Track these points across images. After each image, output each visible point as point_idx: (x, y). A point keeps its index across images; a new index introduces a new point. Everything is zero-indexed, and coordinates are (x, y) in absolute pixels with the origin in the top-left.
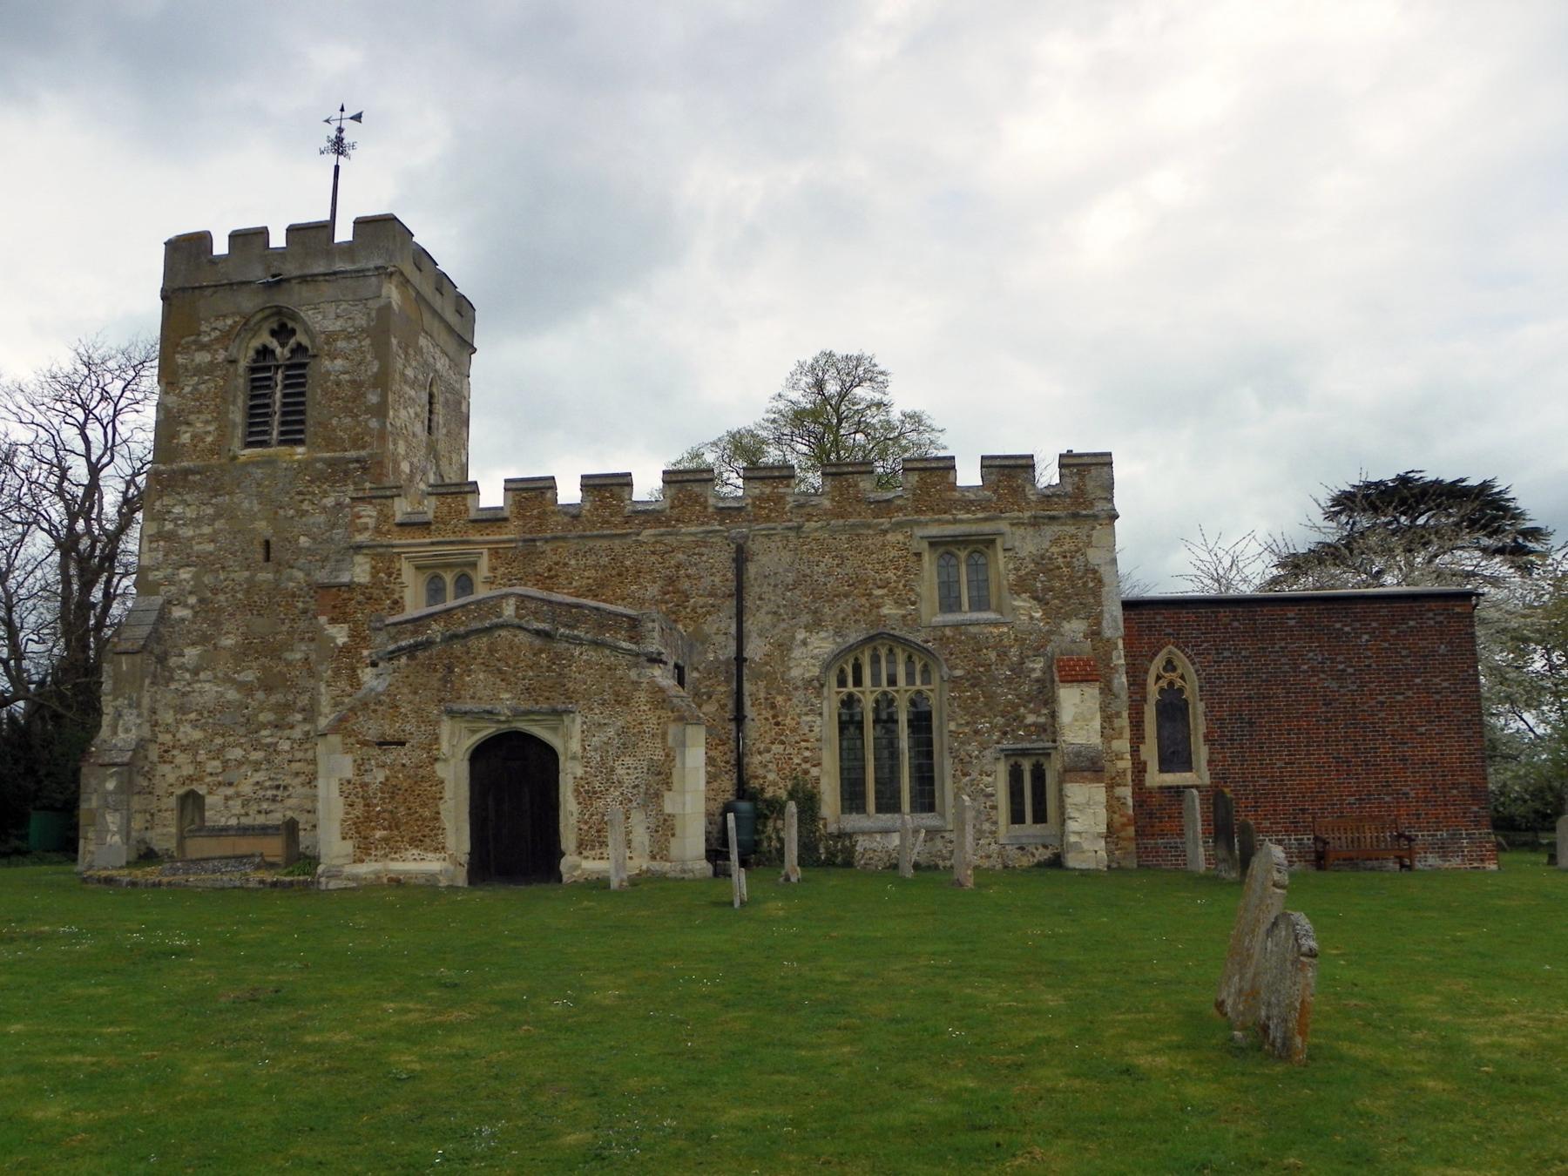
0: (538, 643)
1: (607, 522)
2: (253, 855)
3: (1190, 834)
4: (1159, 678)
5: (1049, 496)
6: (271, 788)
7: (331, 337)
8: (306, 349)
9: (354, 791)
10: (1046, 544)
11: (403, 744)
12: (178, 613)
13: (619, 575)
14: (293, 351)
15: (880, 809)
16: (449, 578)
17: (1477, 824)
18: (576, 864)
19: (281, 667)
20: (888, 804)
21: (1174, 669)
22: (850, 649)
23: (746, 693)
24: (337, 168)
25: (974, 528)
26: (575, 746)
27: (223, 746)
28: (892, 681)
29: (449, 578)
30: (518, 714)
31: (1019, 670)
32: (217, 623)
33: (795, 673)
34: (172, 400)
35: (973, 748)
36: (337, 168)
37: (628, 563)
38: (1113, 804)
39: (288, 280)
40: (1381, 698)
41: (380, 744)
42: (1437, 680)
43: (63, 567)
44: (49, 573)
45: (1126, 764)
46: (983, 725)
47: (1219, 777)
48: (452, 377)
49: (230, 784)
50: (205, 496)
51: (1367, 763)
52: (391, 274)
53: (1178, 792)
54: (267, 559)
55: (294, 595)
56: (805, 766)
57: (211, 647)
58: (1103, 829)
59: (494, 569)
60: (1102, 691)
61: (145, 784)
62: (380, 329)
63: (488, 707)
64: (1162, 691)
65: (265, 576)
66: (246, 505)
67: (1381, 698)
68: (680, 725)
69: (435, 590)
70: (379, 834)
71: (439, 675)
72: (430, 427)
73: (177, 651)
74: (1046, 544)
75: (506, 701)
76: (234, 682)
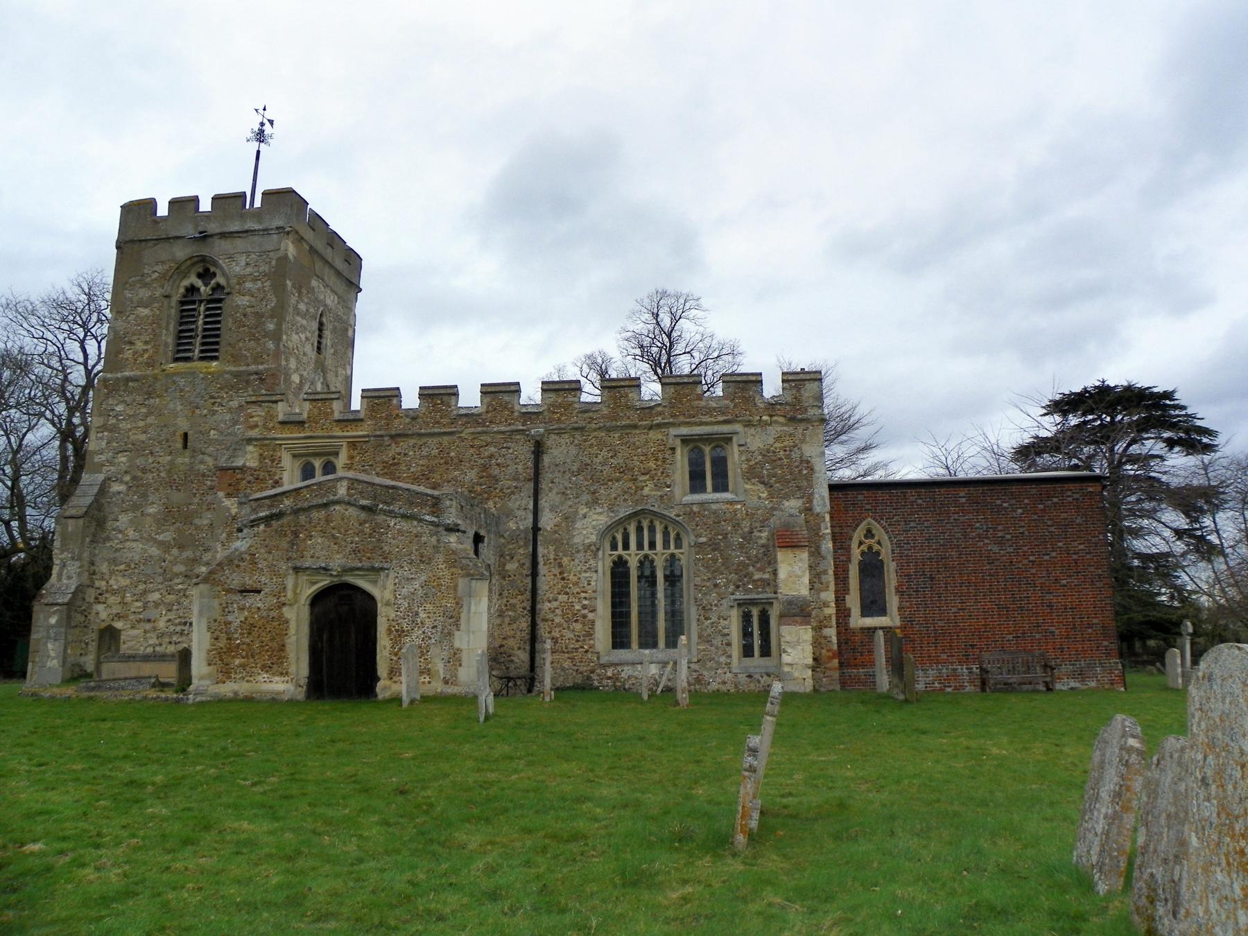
0: (363, 515)
1: (438, 423)
2: (150, 677)
3: (877, 663)
4: (861, 543)
5: (772, 406)
6: (180, 624)
7: (241, 279)
8: (223, 288)
9: (219, 629)
10: (771, 441)
11: (259, 592)
13: (446, 463)
14: (213, 289)
15: (643, 645)
16: (318, 464)
17: (1108, 655)
18: (384, 687)
19: (192, 530)
20: (648, 640)
21: (873, 536)
22: (620, 522)
23: (540, 555)
24: (258, 152)
25: (717, 428)
26: (388, 595)
27: (145, 592)
28: (652, 545)
29: (318, 464)
31: (748, 537)
32: (144, 496)
33: (577, 540)
34: (120, 324)
36: (258, 152)
38: (817, 643)
39: (211, 236)
40: (1032, 558)
41: (241, 592)
42: (1075, 544)
43: (62, 447)
44: (52, 452)
45: (831, 610)
47: (907, 622)
49: (149, 621)
50: (139, 399)
51: (1021, 608)
52: (288, 233)
53: (872, 630)
54: (185, 446)
55: (204, 475)
56: (584, 612)
58: (810, 661)
59: (351, 458)
60: (811, 554)
61: (83, 619)
62: (279, 271)
64: (863, 553)
65: (183, 460)
67: (1032, 558)
68: (467, 579)
69: (308, 472)
70: (237, 662)
72: (319, 348)
73: (112, 516)
74: (771, 441)
75: (337, 561)
76: (155, 540)
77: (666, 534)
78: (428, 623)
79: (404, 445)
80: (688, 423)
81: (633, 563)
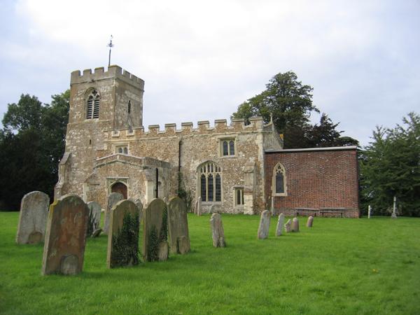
7: (104, 94)
12: (74, 156)
20: (211, 198)
25: (229, 136)
28: (212, 171)
46: (231, 182)
48: (137, 99)
54: (90, 143)
75: (117, 177)
81: (207, 177)
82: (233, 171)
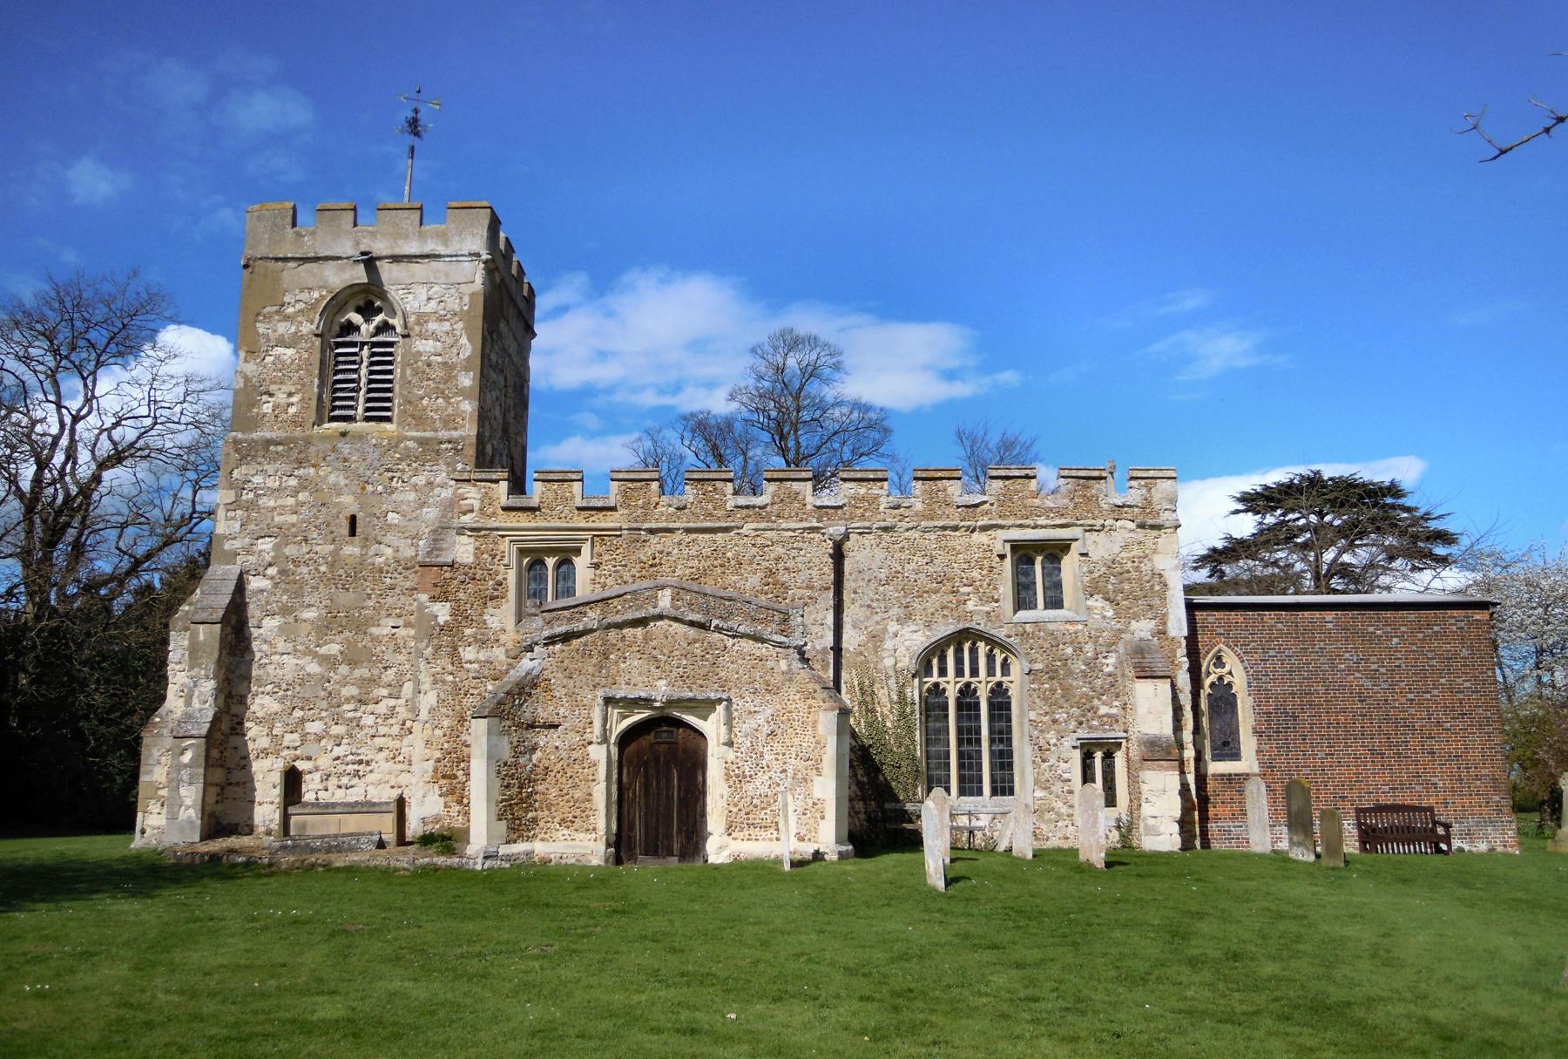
1: (711, 514)
2: (371, 834)
7: (422, 318)
10: (1117, 549)
12: (254, 583)
21: (1223, 665)
27: (303, 721)
28: (974, 672)
30: (670, 703)
31: (1093, 665)
32: (298, 594)
35: (1051, 737)
37: (729, 555)
40: (1411, 696)
46: (1061, 716)
49: (309, 758)
50: (287, 468)
54: (353, 533)
57: (292, 620)
63: (643, 695)
65: (351, 550)
66: (332, 479)
71: (594, 661)
75: (661, 690)
76: (315, 655)
77: (990, 658)
78: (776, 766)
79: (668, 541)
80: (1021, 526)
81: (952, 694)
82: (1070, 673)
